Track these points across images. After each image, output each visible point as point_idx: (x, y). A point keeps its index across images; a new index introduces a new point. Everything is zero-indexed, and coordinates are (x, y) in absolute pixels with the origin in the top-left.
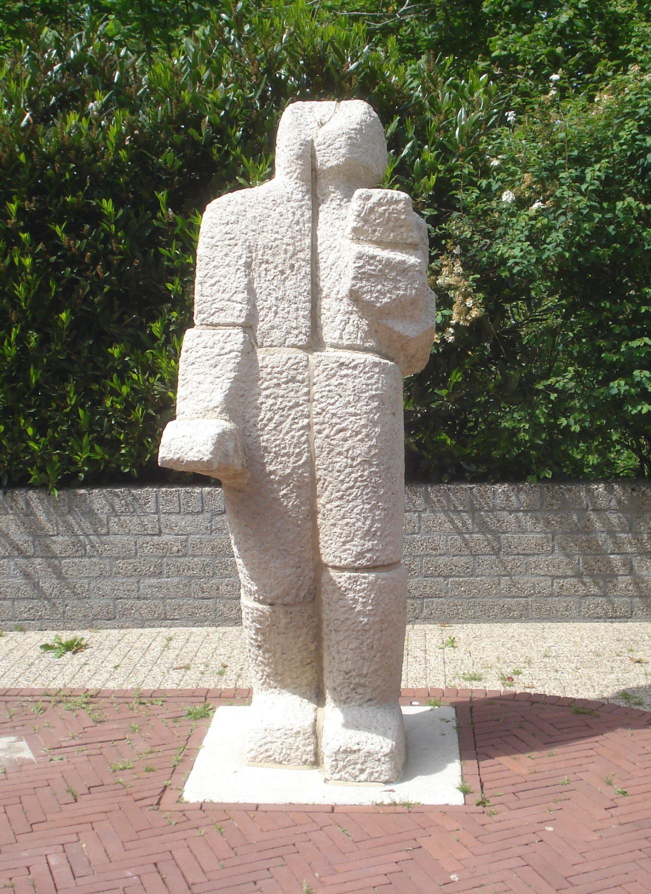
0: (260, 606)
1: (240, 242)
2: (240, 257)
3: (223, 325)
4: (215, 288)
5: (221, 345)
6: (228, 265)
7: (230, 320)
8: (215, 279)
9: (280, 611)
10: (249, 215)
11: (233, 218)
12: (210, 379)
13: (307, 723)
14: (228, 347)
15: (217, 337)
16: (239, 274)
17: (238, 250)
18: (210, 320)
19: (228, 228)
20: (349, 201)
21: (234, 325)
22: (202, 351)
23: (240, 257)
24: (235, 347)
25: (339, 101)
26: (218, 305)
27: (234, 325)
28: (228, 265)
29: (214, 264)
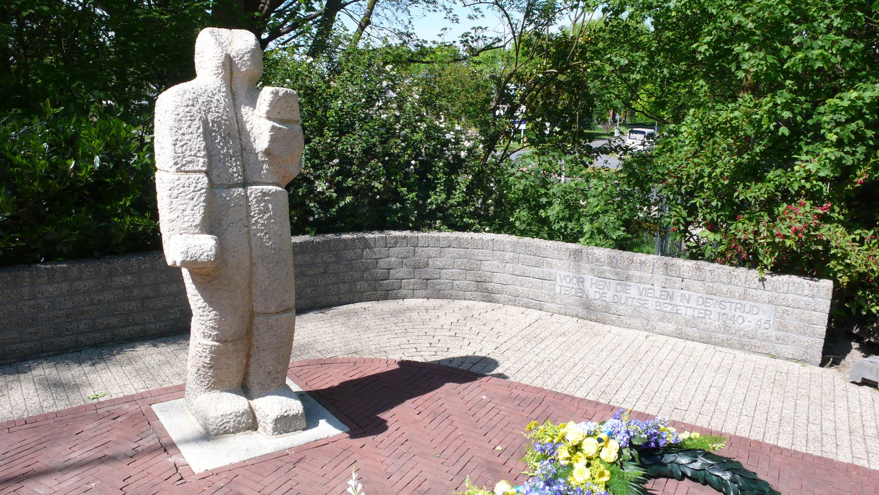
0: (217, 344)
1: (198, 118)
2: (199, 128)
3: (192, 172)
4: (185, 148)
5: (194, 184)
6: (191, 133)
7: (196, 168)
8: (183, 143)
9: (230, 345)
10: (200, 101)
11: (191, 103)
12: (190, 207)
13: (246, 407)
14: (199, 186)
15: (190, 180)
16: (200, 139)
17: (197, 123)
18: (183, 169)
19: (188, 109)
20: (254, 108)
21: (200, 171)
22: (182, 189)
23: (199, 128)
24: (204, 186)
25: (156, 170)
26: (189, 159)
27: (200, 171)
28: (191, 133)
29: (181, 132)
